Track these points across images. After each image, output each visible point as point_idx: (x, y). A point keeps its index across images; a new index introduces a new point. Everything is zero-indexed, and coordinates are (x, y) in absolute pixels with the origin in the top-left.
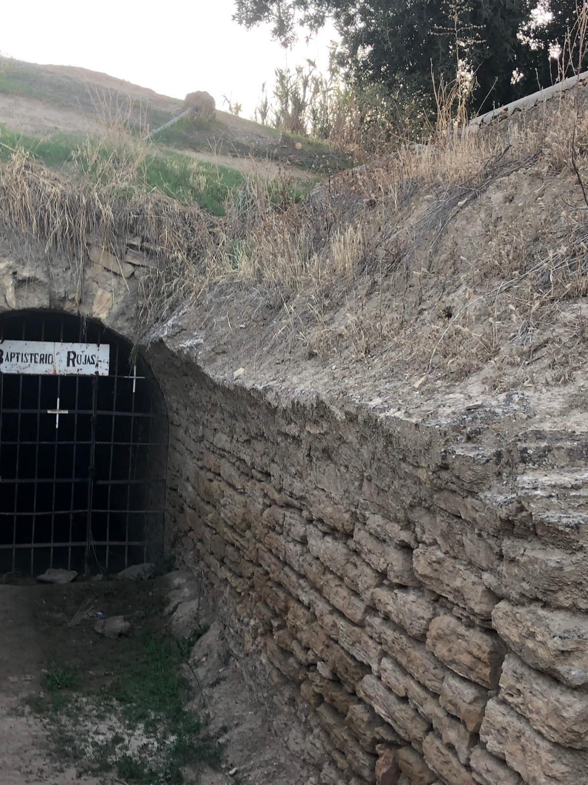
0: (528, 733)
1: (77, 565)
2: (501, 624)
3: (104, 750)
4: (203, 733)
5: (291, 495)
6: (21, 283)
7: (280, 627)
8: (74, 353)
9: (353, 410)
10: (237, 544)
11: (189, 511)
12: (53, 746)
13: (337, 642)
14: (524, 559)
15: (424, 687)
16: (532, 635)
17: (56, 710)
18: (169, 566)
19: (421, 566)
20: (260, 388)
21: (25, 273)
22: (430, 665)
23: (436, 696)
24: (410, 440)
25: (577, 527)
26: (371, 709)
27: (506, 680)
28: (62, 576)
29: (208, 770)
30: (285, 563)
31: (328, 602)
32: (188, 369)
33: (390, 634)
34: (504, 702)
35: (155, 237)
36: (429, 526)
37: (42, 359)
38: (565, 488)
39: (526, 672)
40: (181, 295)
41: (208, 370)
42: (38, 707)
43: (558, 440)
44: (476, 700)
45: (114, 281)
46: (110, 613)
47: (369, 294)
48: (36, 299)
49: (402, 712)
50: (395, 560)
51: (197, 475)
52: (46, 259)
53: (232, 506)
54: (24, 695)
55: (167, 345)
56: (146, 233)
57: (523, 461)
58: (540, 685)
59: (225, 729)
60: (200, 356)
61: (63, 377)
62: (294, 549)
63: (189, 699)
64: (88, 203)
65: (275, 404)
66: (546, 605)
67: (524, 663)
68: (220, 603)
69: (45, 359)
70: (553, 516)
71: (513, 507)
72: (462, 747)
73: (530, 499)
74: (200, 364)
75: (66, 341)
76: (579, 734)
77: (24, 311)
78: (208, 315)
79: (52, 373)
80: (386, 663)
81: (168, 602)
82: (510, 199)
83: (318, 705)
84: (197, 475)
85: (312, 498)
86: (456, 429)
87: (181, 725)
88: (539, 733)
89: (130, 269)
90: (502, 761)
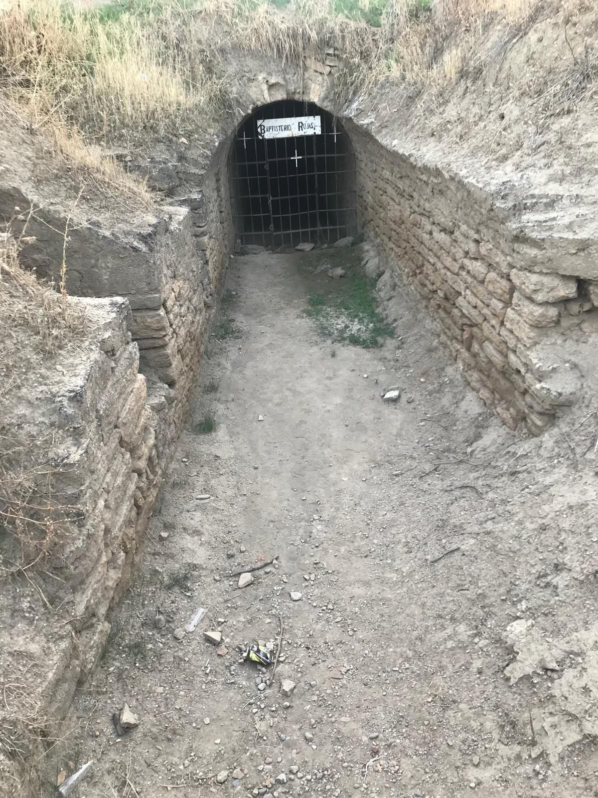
0: (522, 321)
1: (313, 241)
2: (512, 277)
3: (342, 331)
4: (385, 322)
5: (424, 210)
6: (271, 87)
7: (420, 273)
9: (453, 175)
11: (370, 210)
12: (319, 331)
13: (446, 282)
14: (522, 252)
15: (483, 303)
16: (524, 283)
17: (317, 315)
18: (361, 239)
19: (483, 251)
20: (407, 154)
21: (273, 81)
22: (486, 293)
23: (488, 306)
24: (478, 195)
25: (543, 240)
26: (461, 311)
27: (514, 301)
28: (307, 247)
29: (389, 338)
30: (422, 243)
31: (442, 263)
32: (366, 134)
33: (469, 280)
34: (513, 309)
35: (342, 47)
36: (486, 234)
38: (541, 222)
39: (523, 298)
40: (359, 85)
41: (378, 138)
42: (309, 314)
43: (541, 198)
44: (503, 308)
45: (320, 78)
46: (335, 266)
47: (464, 94)
49: (474, 312)
50: (472, 246)
51: (374, 191)
52: (282, 70)
53: (394, 211)
54: (302, 309)
56: (336, 45)
57: (525, 209)
58: (527, 303)
59: (395, 320)
60: (373, 129)
61: (297, 137)
62: (426, 237)
63: (378, 307)
64: (303, 32)
65: (414, 163)
66: (530, 271)
67: (521, 294)
68: (389, 260)
69: (287, 128)
70: (534, 235)
71: (519, 230)
72: (497, 327)
73: (526, 227)
74: (374, 134)
75: (297, 116)
76: (540, 321)
77: (274, 102)
78: (375, 102)
80: (468, 292)
81: (363, 259)
82: (540, 40)
83: (438, 309)
84: (374, 191)
85: (434, 213)
86: (498, 193)
87: (375, 319)
88: (525, 321)
89: (328, 69)
90: (511, 332)
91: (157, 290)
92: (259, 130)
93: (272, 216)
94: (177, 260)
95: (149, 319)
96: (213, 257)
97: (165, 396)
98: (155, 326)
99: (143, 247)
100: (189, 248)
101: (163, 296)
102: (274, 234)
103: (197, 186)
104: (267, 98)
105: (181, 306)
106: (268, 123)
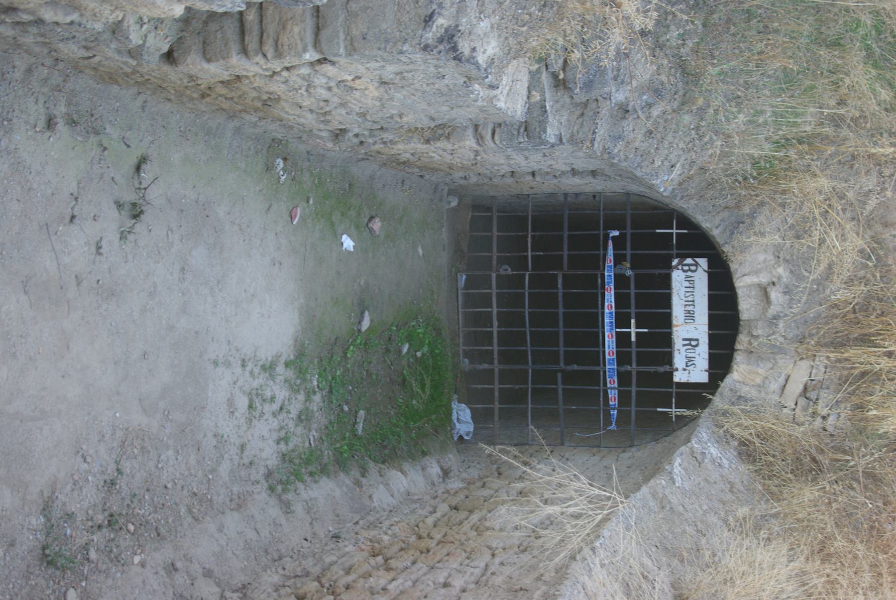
8: (697, 346)
10: (466, 522)
21: (775, 295)
32: (654, 470)
37: (689, 312)
48: (748, 306)
55: (683, 448)
60: (661, 481)
61: (670, 334)
69: (690, 316)
75: (711, 337)
79: (674, 322)
91: (352, 50)
92: (689, 261)
93: (528, 273)
94: (417, 90)
95: (300, 30)
96: (438, 152)
97: (143, 45)
98: (284, 39)
99: (430, 36)
100: (444, 113)
101: (343, 61)
102: (494, 275)
103: (572, 136)
104: (745, 283)
105: (329, 89)
106: (701, 279)
